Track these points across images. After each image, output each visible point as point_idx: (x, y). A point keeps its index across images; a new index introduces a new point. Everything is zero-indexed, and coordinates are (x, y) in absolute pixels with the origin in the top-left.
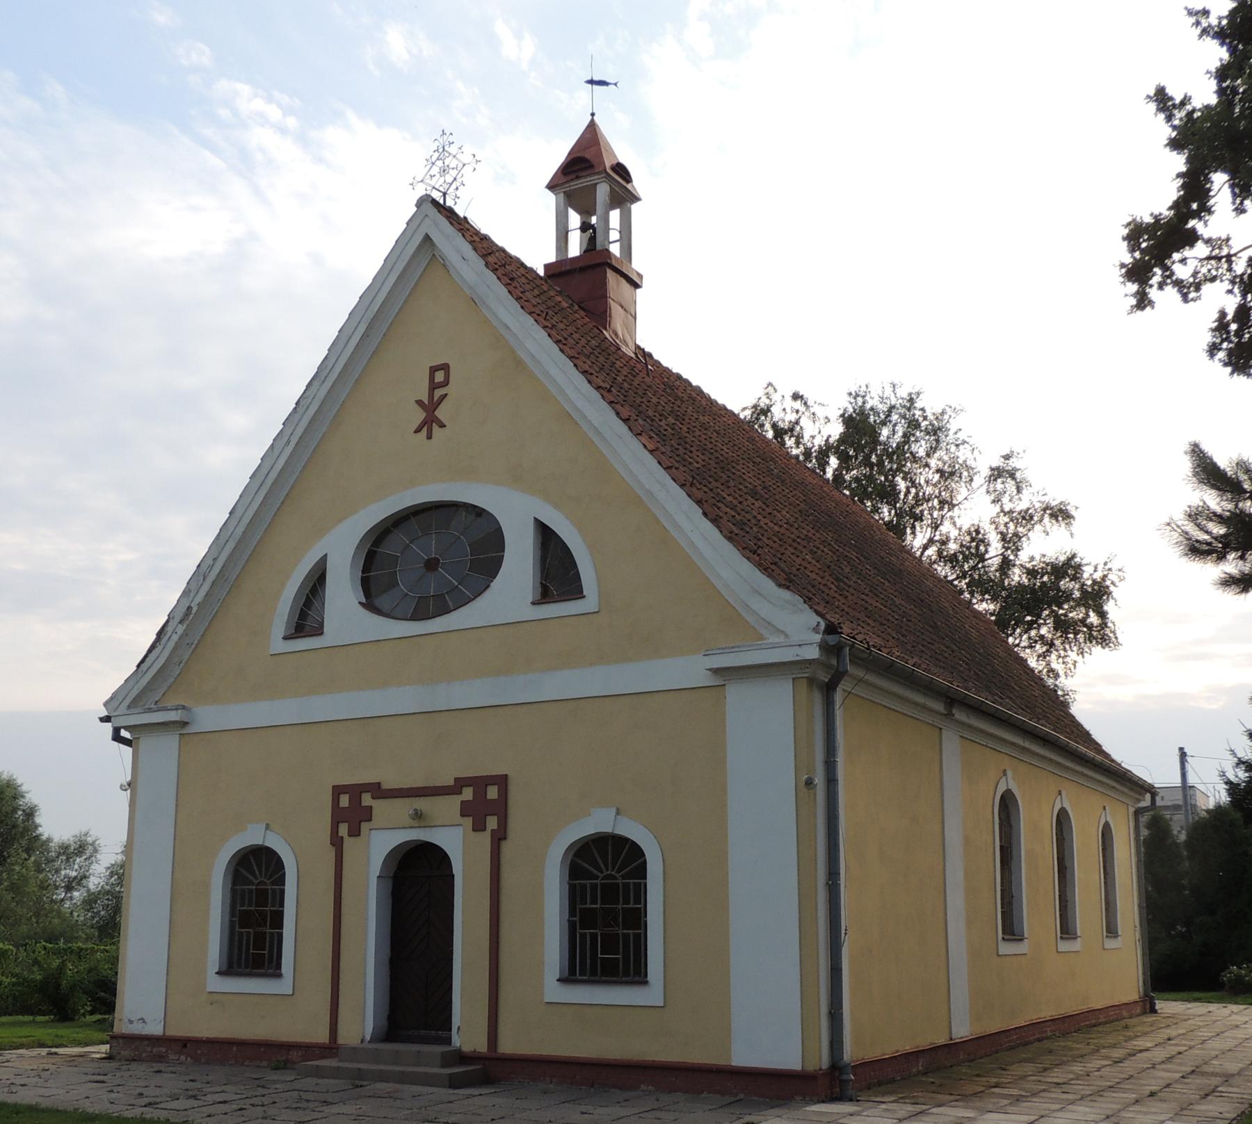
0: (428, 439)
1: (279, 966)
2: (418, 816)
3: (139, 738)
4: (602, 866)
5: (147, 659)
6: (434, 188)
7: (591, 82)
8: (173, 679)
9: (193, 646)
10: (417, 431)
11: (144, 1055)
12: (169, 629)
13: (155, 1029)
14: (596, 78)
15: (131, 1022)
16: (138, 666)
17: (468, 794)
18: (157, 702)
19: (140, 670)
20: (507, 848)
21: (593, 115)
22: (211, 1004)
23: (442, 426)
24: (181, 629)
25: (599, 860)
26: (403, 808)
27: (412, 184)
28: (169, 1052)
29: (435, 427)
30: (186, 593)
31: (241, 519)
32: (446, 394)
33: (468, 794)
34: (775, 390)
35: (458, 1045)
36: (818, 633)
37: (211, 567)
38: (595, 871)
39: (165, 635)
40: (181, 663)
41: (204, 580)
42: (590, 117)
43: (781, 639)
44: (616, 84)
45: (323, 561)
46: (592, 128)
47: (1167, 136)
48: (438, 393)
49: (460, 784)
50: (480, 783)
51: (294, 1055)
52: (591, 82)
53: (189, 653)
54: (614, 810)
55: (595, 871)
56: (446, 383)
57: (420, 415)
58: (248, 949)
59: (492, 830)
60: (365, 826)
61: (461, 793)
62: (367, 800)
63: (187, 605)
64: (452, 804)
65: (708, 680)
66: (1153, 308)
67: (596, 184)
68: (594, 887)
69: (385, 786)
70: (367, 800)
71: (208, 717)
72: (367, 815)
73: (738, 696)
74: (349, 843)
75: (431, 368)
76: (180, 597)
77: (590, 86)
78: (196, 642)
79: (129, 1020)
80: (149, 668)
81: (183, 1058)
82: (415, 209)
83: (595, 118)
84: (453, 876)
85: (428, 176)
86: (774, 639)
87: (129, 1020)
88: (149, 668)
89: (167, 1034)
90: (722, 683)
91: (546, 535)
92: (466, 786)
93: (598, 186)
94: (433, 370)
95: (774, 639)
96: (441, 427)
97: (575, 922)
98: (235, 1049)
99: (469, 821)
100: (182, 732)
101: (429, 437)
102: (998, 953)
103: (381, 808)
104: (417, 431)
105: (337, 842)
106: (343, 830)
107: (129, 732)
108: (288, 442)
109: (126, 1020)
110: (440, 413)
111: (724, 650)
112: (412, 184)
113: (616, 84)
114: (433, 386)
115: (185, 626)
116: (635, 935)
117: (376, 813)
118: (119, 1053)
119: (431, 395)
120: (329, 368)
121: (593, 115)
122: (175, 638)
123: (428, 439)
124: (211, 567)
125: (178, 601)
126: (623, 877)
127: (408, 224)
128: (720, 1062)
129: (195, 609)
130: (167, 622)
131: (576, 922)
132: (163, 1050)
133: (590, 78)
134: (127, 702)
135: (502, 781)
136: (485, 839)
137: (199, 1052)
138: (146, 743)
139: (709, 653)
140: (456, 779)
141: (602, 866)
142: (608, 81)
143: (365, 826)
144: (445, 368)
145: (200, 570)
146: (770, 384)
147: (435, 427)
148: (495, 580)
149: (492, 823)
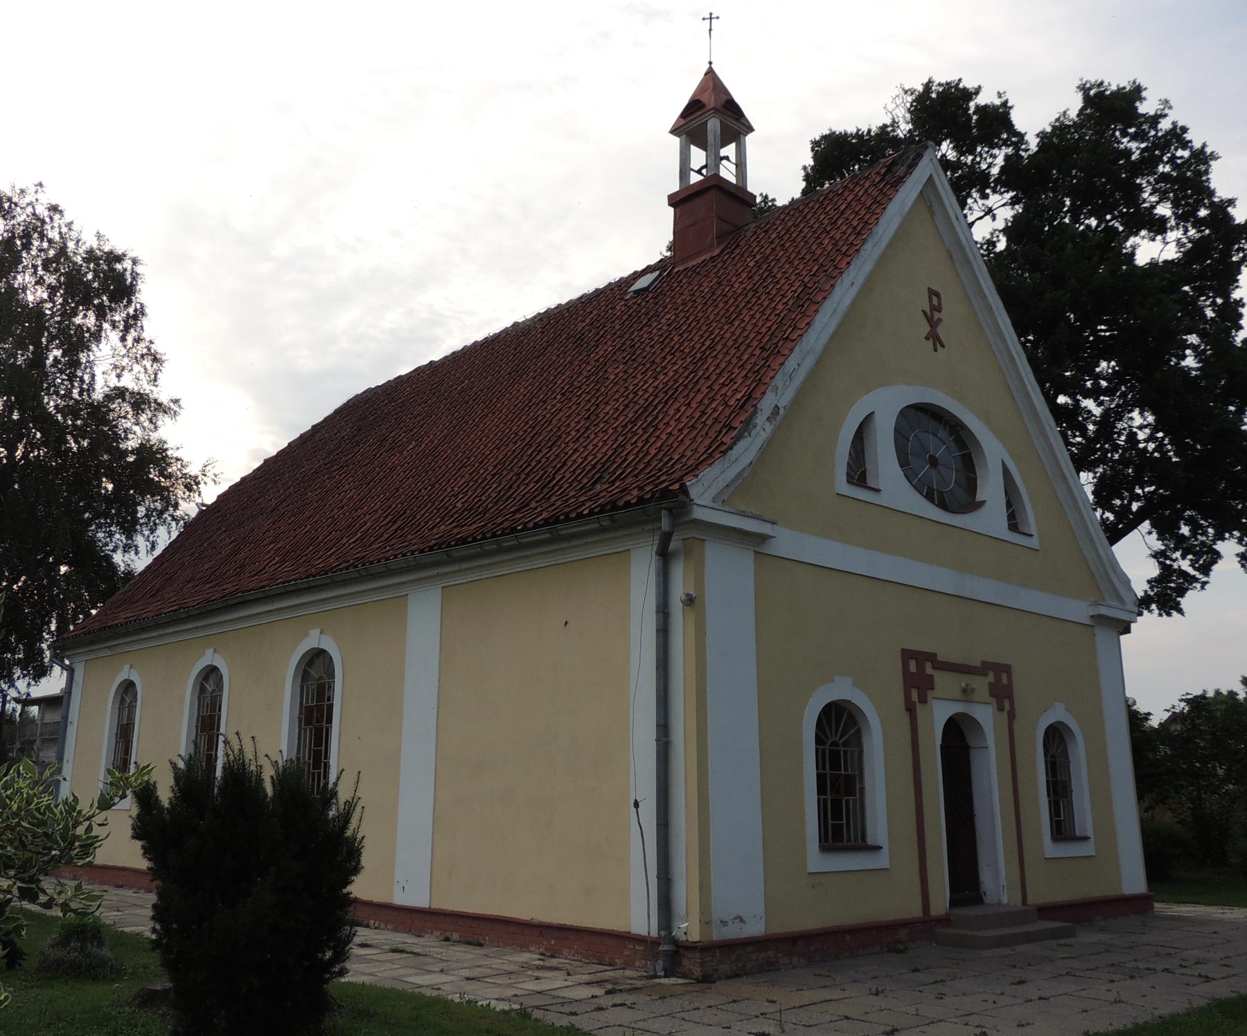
11: (749, 966)
13: (755, 928)
15: (724, 923)
20: (1016, 725)
21: (710, 63)
28: (779, 955)
42: (708, 65)
45: (870, 416)
51: (903, 934)
60: (930, 694)
62: (929, 670)
65: (1089, 622)
69: (940, 658)
70: (929, 670)
71: (787, 542)
74: (919, 707)
79: (722, 922)
81: (795, 960)
83: (712, 66)
87: (722, 922)
89: (433, 907)
92: (1124, 694)
98: (848, 938)
100: (757, 550)
103: (943, 680)
105: (910, 709)
106: (915, 696)
109: (719, 923)
116: (848, 771)
118: (717, 970)
121: (710, 63)
129: (782, 411)
132: (771, 954)
136: (1005, 715)
137: (812, 949)
149: (1007, 703)
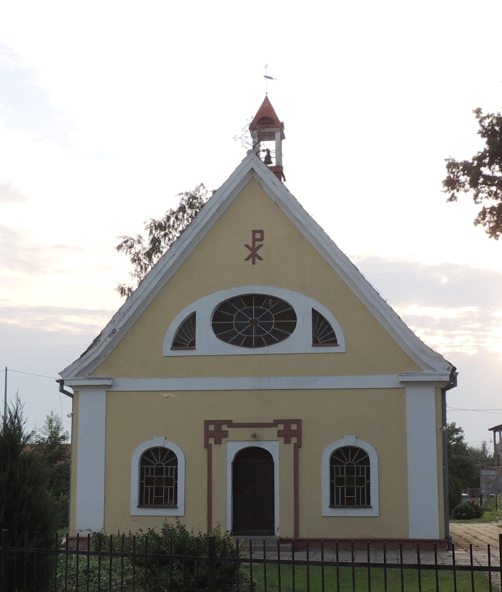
0: (253, 264)
1: (176, 502)
2: (254, 436)
3: (78, 391)
4: (346, 459)
5: (88, 353)
6: (247, 143)
7: (266, 77)
8: (101, 364)
9: (113, 348)
10: (247, 259)
12: (102, 339)
14: (268, 75)
16: (82, 356)
17: (281, 427)
18: (90, 374)
19: (82, 358)
20: (301, 451)
22: (134, 521)
23: (261, 259)
24: (109, 340)
25: (345, 457)
26: (248, 432)
27: (234, 138)
29: (257, 259)
30: (112, 322)
31: (146, 288)
32: (262, 245)
33: (281, 427)
34: (204, 188)
35: (279, 535)
36: (449, 371)
37: (128, 311)
38: (343, 462)
39: (99, 342)
40: (105, 356)
41: (123, 317)
43: (431, 372)
44: (276, 79)
46: (266, 101)
47: (479, 129)
48: (257, 243)
49: (276, 423)
50: (288, 423)
52: (266, 77)
53: (111, 351)
54: (355, 437)
55: (343, 462)
56: (262, 239)
57: (248, 253)
58: (152, 495)
59: (294, 443)
61: (277, 427)
63: (114, 328)
64: (273, 431)
66: (456, 201)
67: (275, 132)
68: (152, 469)
69: (235, 421)
72: (225, 434)
73: (411, 393)
74: (215, 448)
75: (253, 231)
76: (109, 323)
77: (266, 78)
78: (115, 346)
80: (89, 357)
82: (246, 155)
84: (274, 463)
85: (244, 136)
86: (426, 371)
88: (89, 357)
90: (404, 387)
91: (317, 317)
93: (276, 133)
94: (254, 232)
95: (426, 371)
96: (260, 259)
97: (333, 483)
99: (282, 439)
101: (254, 263)
102: (184, 516)
104: (247, 259)
105: (208, 447)
107: (72, 388)
108: (174, 255)
110: (259, 252)
111: (407, 374)
112: (234, 138)
113: (276, 79)
114: (254, 240)
115: (112, 338)
117: (230, 434)
119: (254, 244)
120: (198, 222)
122: (106, 344)
123: (253, 264)
124: (128, 311)
125: (107, 325)
126: (166, 465)
127: (242, 161)
128: (404, 537)
130: (100, 335)
131: (172, 488)
133: (265, 75)
134: (76, 372)
135: (299, 422)
138: (83, 396)
139: (401, 375)
140: (275, 420)
141: (346, 459)
142: (272, 77)
143: (224, 440)
144: (261, 232)
145: (121, 311)
146: (202, 184)
147: (257, 259)
148: (292, 335)
149: (294, 440)
